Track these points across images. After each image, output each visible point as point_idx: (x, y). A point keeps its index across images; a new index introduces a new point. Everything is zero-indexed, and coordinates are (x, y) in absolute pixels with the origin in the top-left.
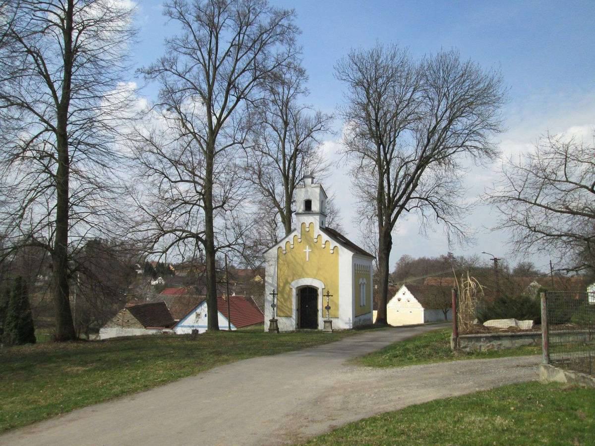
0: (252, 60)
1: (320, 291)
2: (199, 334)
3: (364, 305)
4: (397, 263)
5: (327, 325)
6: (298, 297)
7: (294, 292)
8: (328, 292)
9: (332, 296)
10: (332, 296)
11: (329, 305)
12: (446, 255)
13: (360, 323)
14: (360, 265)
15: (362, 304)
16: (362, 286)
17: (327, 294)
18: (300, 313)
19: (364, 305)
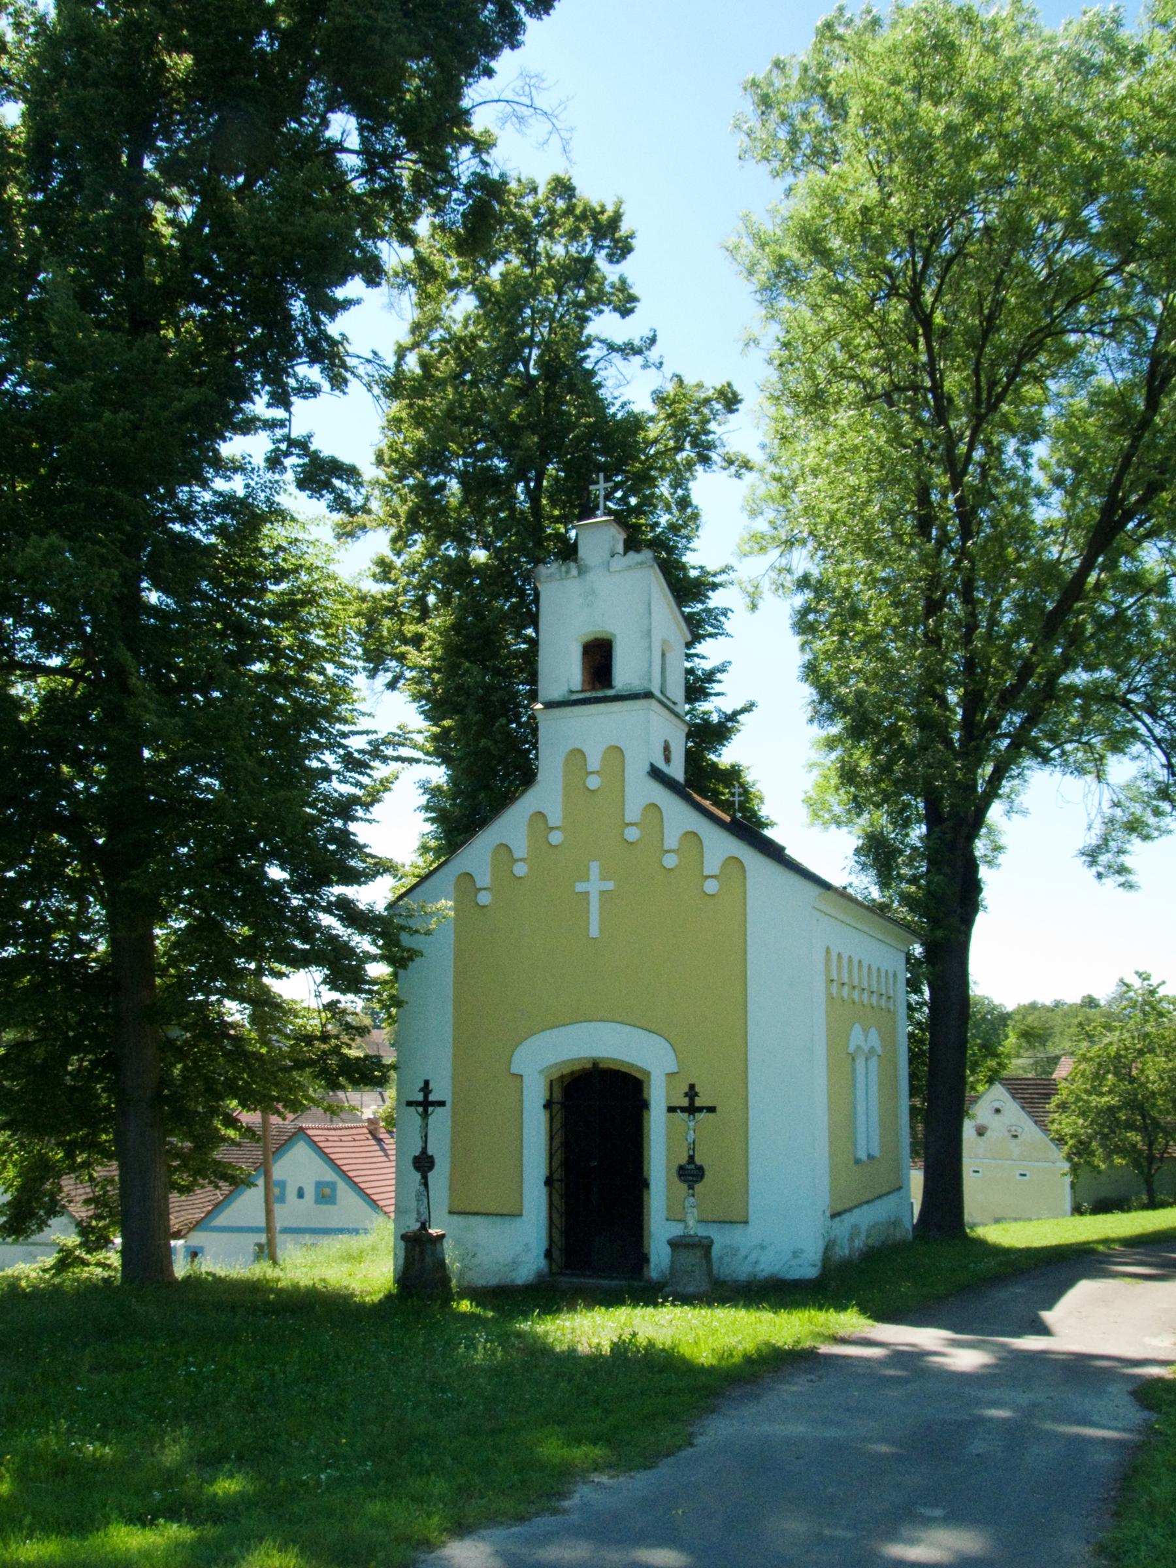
0: (1005, 389)
1: (658, 1096)
2: (424, 372)
3: (871, 1157)
4: (548, 14)
5: (691, 1259)
6: (551, 1119)
7: (535, 1094)
8: (692, 1093)
9: (712, 1110)
10: (712, 1110)
11: (698, 1160)
12: (551, 12)
13: (856, 1243)
14: (869, 967)
15: (862, 1155)
16: (860, 1064)
17: (685, 1102)
18: (557, 1124)
19: (871, 1157)
